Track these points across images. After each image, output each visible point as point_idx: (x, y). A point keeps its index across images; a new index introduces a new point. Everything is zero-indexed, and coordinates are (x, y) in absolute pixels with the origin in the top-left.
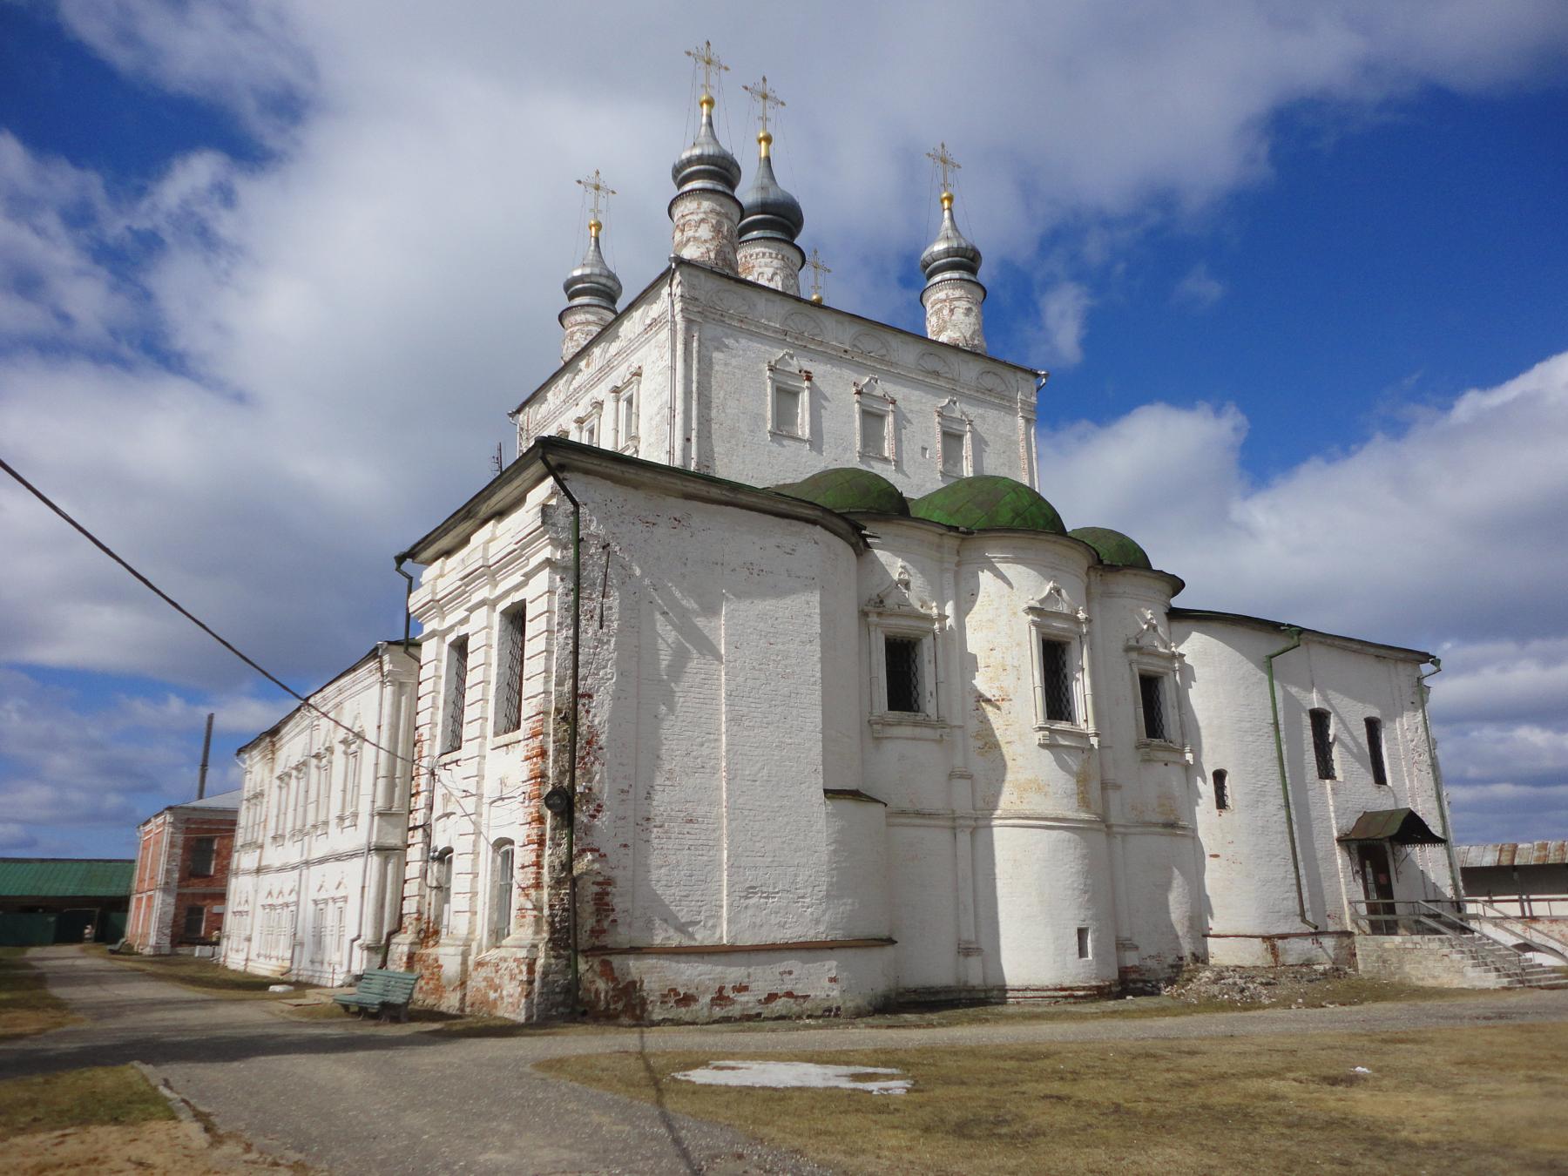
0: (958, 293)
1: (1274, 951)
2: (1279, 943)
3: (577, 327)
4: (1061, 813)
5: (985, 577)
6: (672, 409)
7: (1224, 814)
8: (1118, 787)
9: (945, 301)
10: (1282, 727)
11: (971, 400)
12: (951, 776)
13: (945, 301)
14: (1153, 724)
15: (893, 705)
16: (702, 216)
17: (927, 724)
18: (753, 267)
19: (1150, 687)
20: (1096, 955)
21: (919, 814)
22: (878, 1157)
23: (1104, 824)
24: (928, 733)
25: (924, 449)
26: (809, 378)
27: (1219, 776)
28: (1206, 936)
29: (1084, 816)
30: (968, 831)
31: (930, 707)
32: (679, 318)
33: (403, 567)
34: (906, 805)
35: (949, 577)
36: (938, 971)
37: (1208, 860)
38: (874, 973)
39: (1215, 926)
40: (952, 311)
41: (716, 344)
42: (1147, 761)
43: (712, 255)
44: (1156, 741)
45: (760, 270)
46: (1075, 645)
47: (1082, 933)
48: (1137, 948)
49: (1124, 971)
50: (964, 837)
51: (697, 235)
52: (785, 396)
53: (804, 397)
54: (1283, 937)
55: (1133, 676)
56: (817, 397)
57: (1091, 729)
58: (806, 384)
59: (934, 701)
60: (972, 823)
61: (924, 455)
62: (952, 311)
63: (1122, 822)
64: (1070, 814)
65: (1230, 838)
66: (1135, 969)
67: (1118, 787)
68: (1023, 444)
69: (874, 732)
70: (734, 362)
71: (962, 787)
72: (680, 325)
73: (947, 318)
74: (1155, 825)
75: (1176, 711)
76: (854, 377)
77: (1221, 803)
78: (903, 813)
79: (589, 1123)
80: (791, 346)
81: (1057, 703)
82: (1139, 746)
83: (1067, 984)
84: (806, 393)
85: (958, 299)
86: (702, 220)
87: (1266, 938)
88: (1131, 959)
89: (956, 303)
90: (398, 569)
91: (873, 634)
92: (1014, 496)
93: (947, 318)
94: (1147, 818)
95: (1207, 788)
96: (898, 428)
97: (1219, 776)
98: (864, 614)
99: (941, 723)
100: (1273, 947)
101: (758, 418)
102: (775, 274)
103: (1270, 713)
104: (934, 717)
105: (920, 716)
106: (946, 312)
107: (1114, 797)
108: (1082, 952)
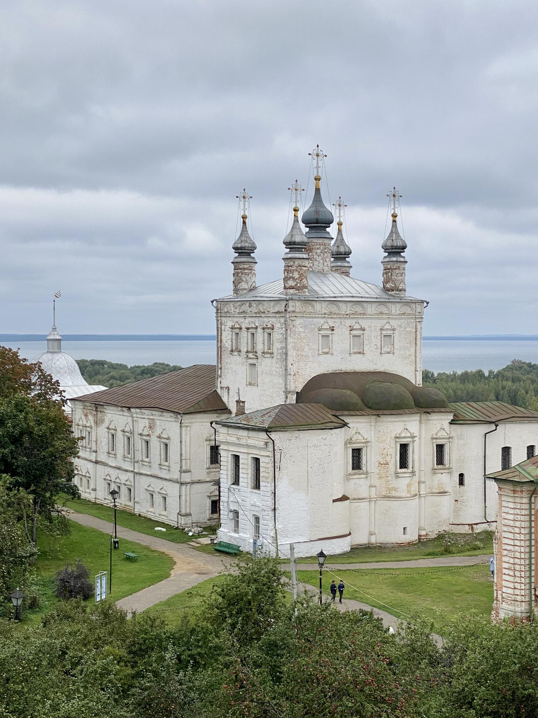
2: (475, 526)
3: (240, 271)
7: (462, 487)
8: (424, 482)
9: (390, 269)
12: (370, 486)
13: (390, 269)
14: (440, 460)
15: (353, 469)
18: (313, 249)
19: (440, 448)
22: (197, 592)
24: (363, 476)
30: (374, 502)
31: (364, 468)
33: (212, 425)
34: (355, 497)
41: (301, 326)
44: (440, 466)
48: (425, 530)
51: (293, 276)
55: (433, 447)
59: (365, 467)
60: (375, 499)
63: (425, 493)
66: (423, 535)
67: (424, 482)
69: (347, 478)
71: (373, 489)
74: (436, 493)
75: (448, 456)
78: (355, 499)
79: (22, 434)
82: (434, 469)
83: (399, 542)
88: (423, 533)
90: (211, 426)
91: (348, 450)
94: (433, 491)
98: (346, 444)
99: (367, 473)
100: (472, 528)
104: (365, 471)
106: (390, 274)
107: (422, 486)
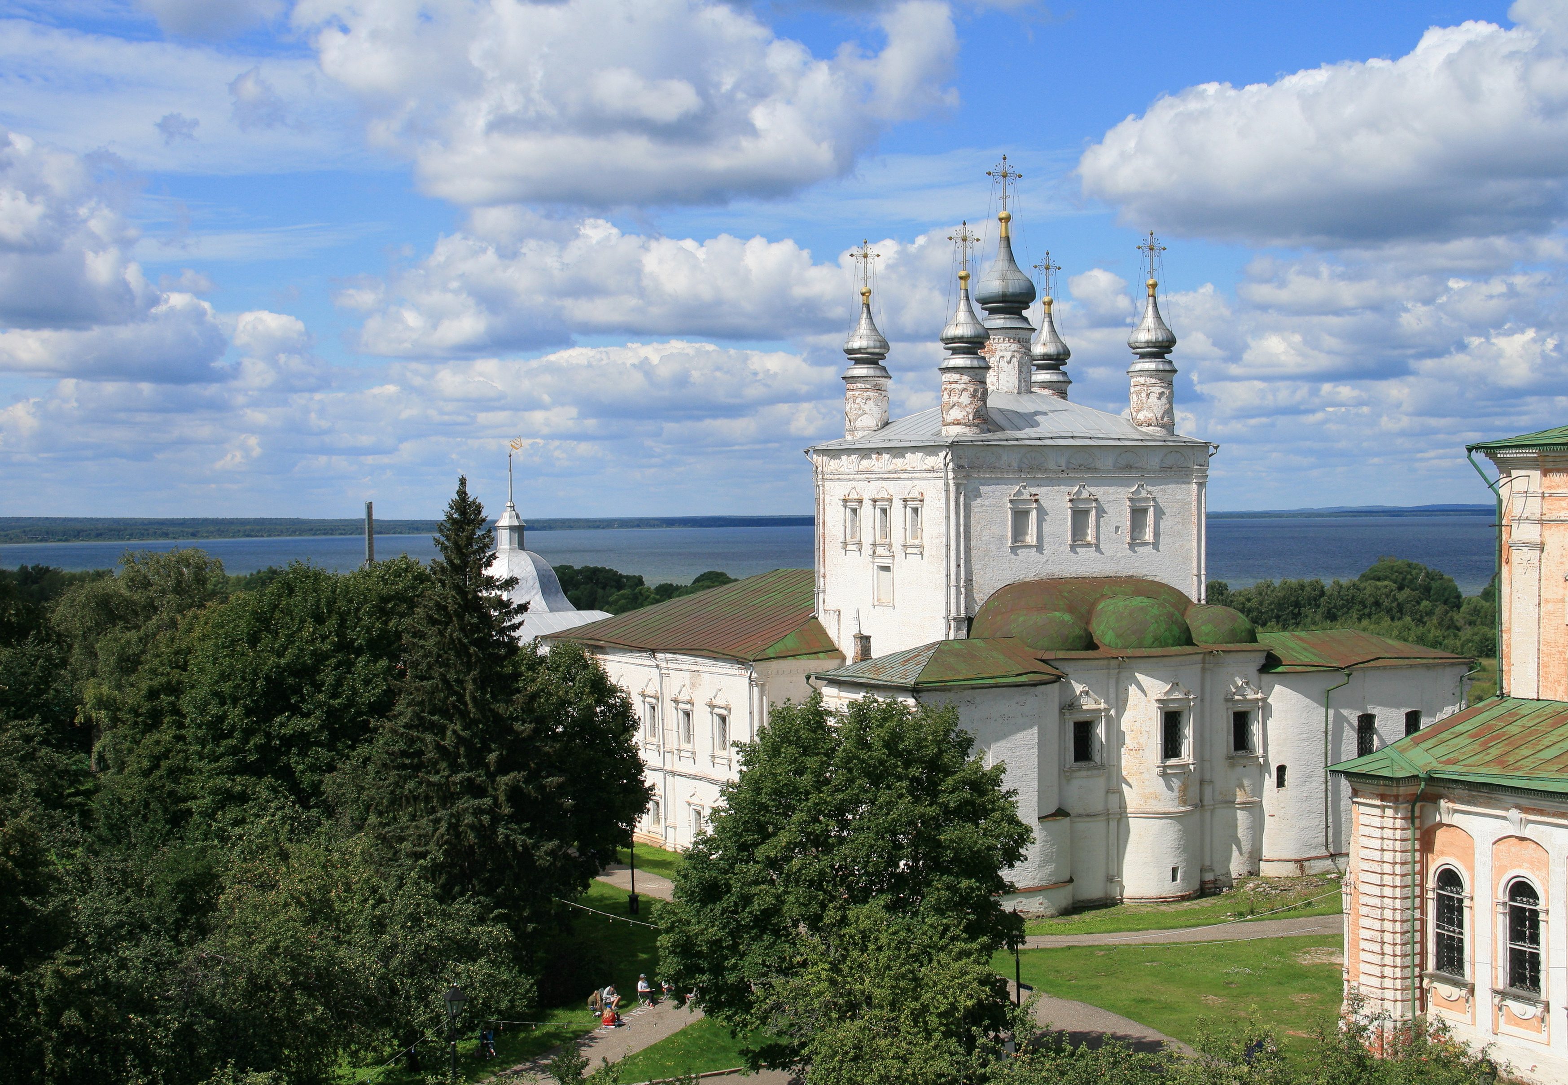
0: (1153, 381)
1: (1302, 868)
4: (1166, 810)
5: (1133, 690)
6: (948, 546)
10: (1330, 733)
11: (1154, 483)
15: (1077, 759)
16: (963, 386)
17: (1096, 768)
20: (1183, 880)
21: (1088, 816)
23: (1200, 805)
25: (1117, 528)
26: (1036, 501)
27: (1281, 769)
28: (1261, 860)
29: (1182, 809)
31: (1097, 758)
32: (951, 482)
34: (1081, 811)
35: (1112, 682)
36: (1093, 890)
37: (1267, 817)
38: (1064, 897)
39: (1266, 853)
40: (1148, 395)
42: (1233, 766)
43: (971, 417)
45: (1001, 354)
46: (1186, 713)
47: (1175, 870)
49: (1203, 883)
50: (1113, 824)
52: (1020, 516)
53: (1033, 515)
54: (1308, 860)
56: (1042, 514)
57: (1191, 761)
58: (1035, 505)
61: (1116, 532)
62: (1148, 395)
64: (1172, 810)
65: (1282, 805)
68: (1195, 503)
69: (1065, 775)
70: (987, 503)
72: (952, 488)
73: (1144, 400)
76: (1068, 489)
77: (1281, 783)
78: (1080, 816)
80: (1024, 480)
81: (1171, 747)
84: (1035, 512)
85: (1153, 385)
86: (964, 390)
87: (1296, 861)
89: (1152, 389)
92: (1156, 625)
93: (1144, 400)
95: (1270, 781)
96: (1098, 518)
97: (1281, 769)
101: (1002, 538)
102: (1013, 357)
103: (1324, 725)
105: (1092, 764)
106: (1144, 395)
108: (1174, 879)
